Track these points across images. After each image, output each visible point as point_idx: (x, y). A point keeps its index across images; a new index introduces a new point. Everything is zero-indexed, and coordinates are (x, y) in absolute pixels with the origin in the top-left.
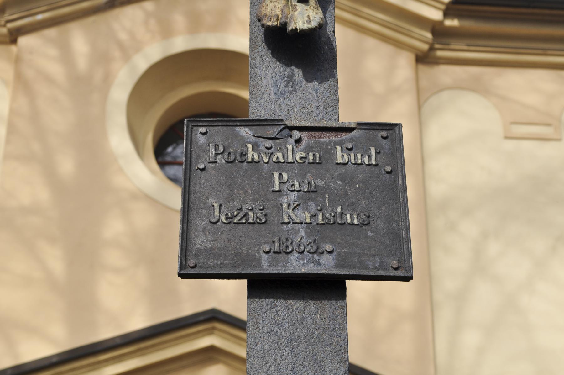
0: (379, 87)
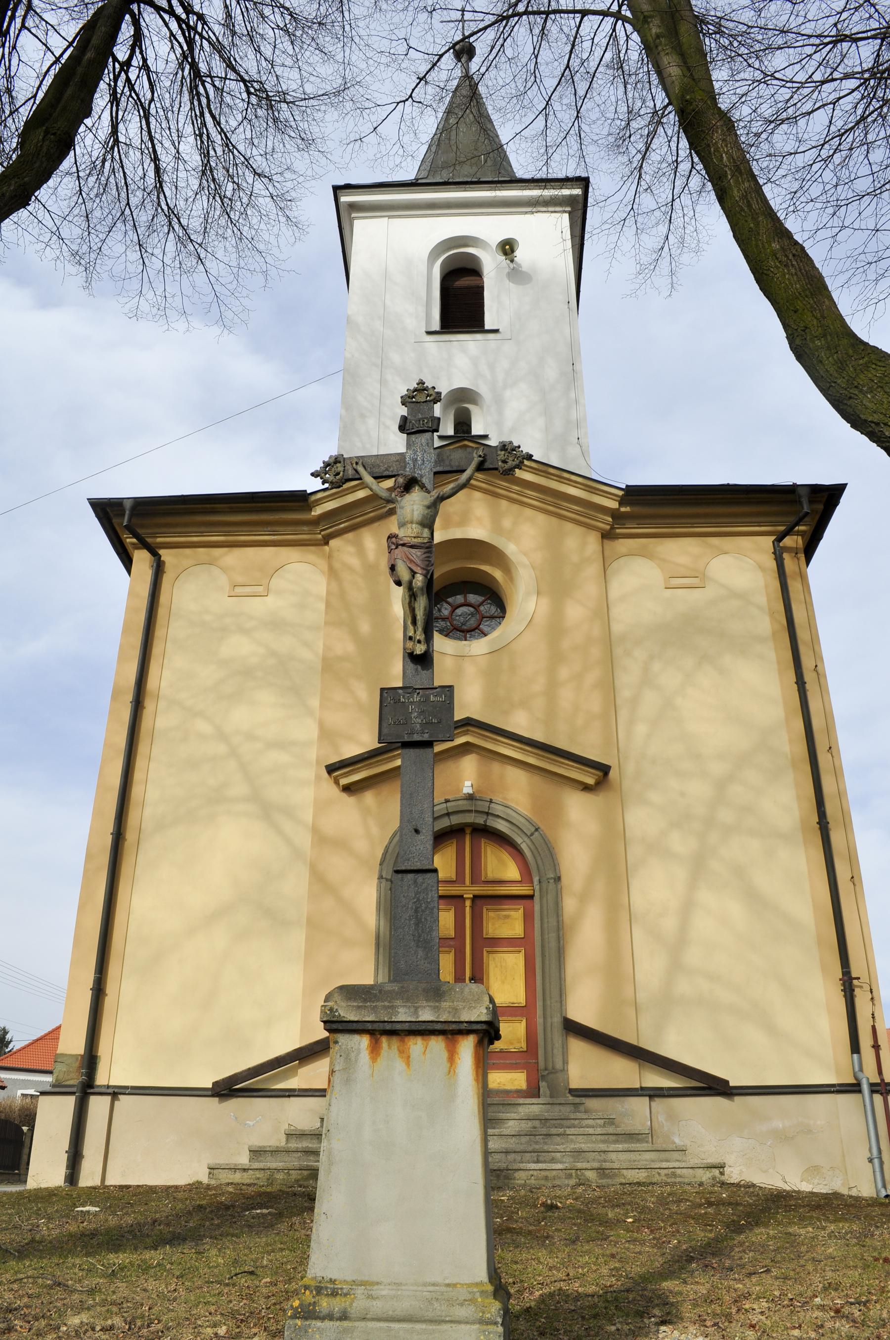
0: (575, 558)
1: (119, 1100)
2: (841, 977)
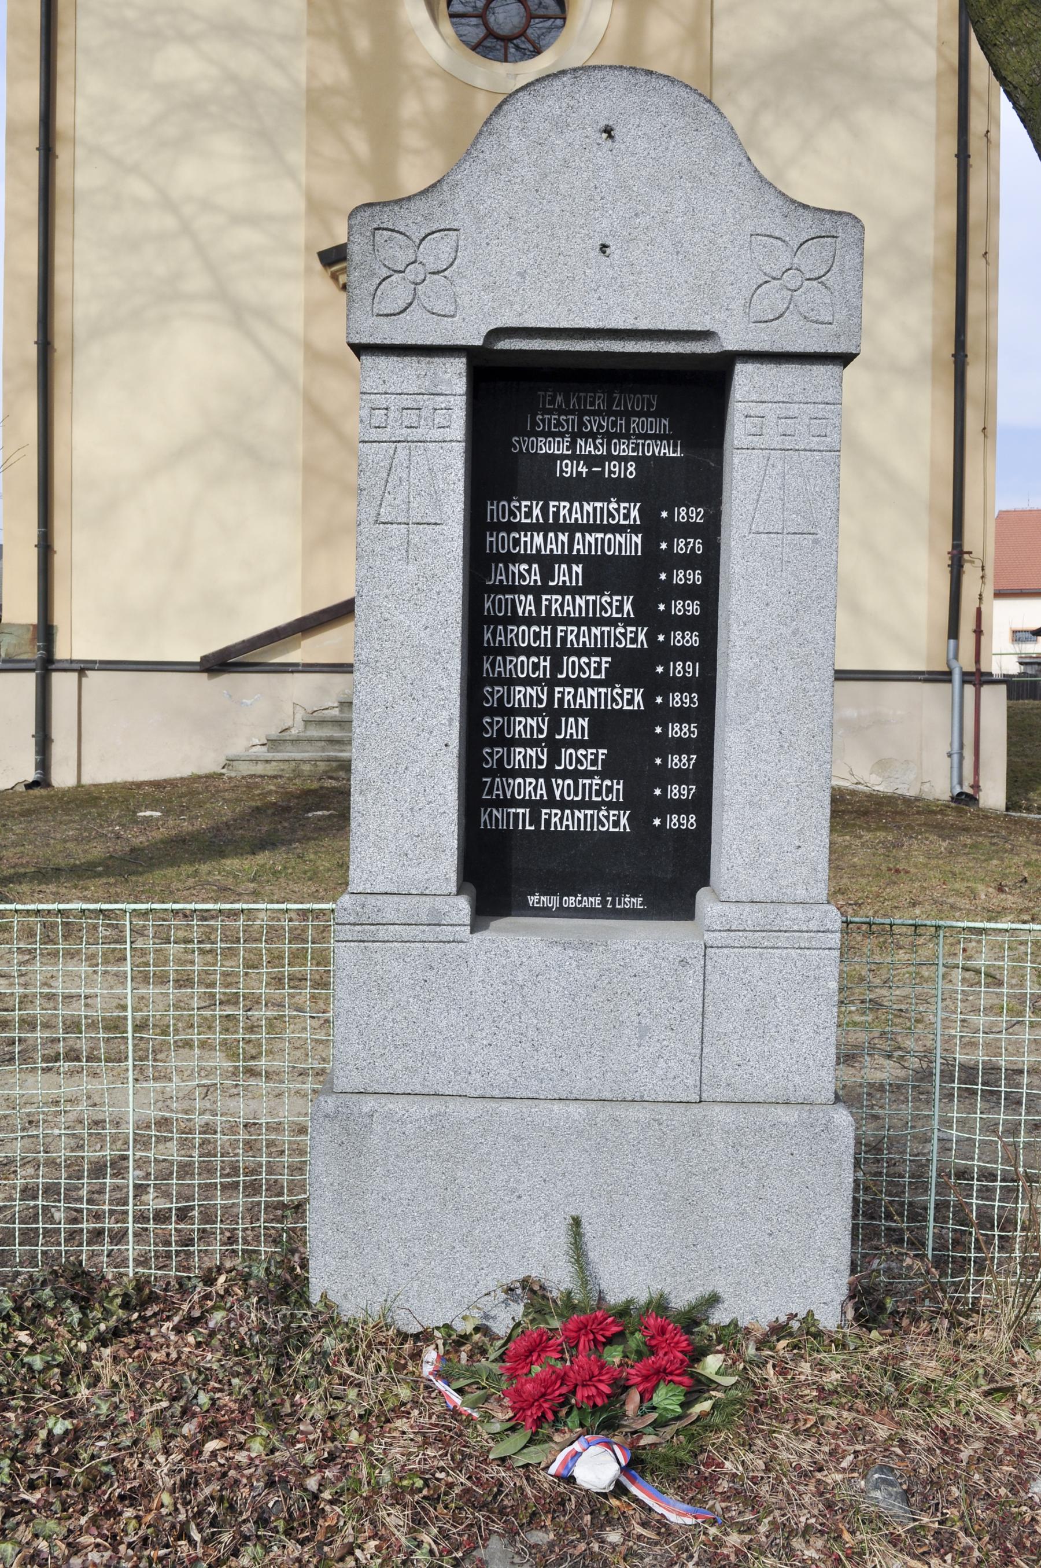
1: (86, 676)
2: (950, 549)
